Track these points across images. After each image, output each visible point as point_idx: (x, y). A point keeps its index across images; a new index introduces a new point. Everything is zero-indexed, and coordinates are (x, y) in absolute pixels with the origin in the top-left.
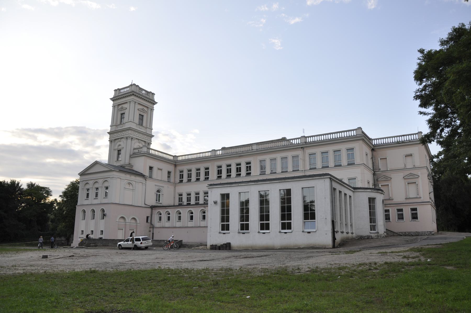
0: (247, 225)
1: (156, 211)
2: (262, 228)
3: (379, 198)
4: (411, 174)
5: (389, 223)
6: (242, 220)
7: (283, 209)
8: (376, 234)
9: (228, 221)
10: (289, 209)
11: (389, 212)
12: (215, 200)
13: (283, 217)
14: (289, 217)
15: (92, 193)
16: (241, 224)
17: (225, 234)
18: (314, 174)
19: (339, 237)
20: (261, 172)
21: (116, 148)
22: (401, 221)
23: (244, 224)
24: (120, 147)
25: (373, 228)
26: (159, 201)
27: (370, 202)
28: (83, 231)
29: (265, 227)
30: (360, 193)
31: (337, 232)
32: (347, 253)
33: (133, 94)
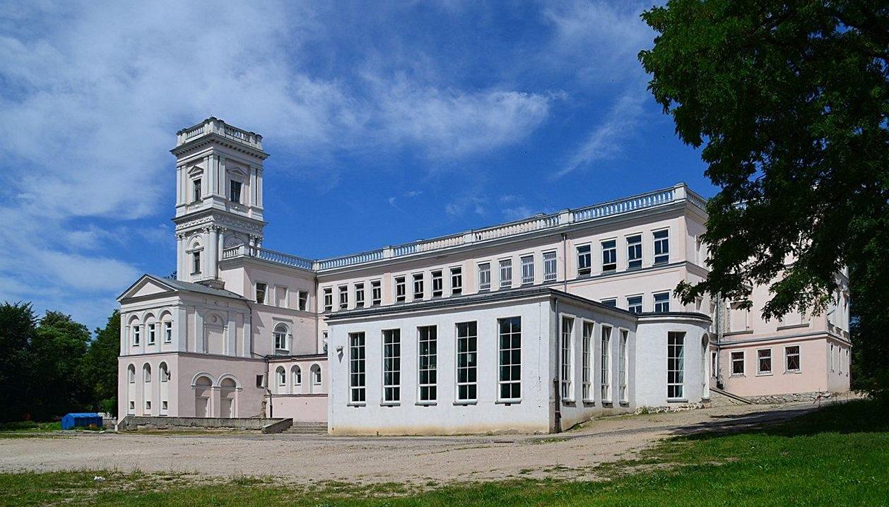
1: (273, 367)
2: (505, 394)
3: (693, 335)
5: (741, 379)
6: (355, 384)
7: (505, 358)
8: (683, 404)
9: (473, 378)
12: (339, 345)
13: (504, 375)
14: (517, 374)
15: (145, 333)
16: (503, 385)
17: (465, 405)
20: (503, 284)
21: (191, 248)
24: (197, 247)
25: (673, 392)
26: (283, 347)
28: (133, 403)
29: (429, 394)
31: (568, 404)
33: (213, 141)
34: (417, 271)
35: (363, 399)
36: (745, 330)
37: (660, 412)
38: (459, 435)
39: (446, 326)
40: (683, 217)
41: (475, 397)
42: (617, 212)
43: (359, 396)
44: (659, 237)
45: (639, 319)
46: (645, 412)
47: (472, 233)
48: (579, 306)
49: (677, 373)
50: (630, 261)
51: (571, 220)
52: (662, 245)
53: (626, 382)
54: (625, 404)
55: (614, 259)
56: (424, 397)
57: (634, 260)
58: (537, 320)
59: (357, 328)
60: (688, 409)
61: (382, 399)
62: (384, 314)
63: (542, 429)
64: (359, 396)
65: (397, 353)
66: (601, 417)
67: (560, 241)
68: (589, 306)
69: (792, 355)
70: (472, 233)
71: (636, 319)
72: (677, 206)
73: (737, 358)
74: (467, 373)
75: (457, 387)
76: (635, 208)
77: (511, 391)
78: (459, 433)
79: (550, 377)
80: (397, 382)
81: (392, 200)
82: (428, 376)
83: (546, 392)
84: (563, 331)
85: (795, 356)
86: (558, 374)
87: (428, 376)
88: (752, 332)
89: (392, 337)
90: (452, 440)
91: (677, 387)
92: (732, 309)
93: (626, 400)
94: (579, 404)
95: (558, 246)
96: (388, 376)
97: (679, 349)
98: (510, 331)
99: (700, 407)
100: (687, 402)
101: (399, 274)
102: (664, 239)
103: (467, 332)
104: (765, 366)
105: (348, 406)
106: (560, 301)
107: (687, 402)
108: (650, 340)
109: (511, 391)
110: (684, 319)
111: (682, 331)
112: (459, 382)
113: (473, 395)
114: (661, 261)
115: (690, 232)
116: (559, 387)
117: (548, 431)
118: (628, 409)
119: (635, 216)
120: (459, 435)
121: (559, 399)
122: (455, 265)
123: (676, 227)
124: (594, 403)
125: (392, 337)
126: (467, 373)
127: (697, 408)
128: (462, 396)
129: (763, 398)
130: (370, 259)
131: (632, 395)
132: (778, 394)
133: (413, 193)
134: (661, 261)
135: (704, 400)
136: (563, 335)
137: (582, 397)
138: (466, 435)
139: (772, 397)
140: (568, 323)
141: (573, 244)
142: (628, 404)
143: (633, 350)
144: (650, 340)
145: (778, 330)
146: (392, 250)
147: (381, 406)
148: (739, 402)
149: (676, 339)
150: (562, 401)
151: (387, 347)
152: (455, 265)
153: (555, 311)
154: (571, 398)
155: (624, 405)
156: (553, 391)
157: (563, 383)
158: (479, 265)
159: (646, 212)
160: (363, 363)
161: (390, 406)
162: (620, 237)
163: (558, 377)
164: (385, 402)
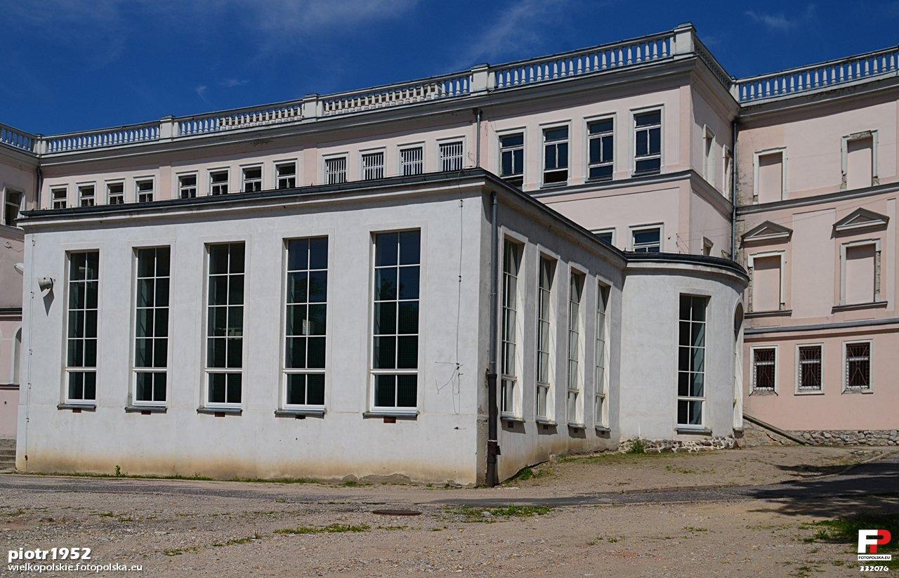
0: (236, 380)
2: (383, 398)
3: (721, 300)
4: (770, 227)
7: (384, 319)
8: (702, 438)
9: (236, 361)
10: (410, 319)
11: (819, 357)
13: (383, 356)
14: (410, 356)
17: (301, 416)
18: (574, 185)
19: (513, 448)
22: (809, 389)
23: (150, 374)
25: (688, 412)
27: (684, 314)
29: (307, 391)
30: (280, 259)
31: (512, 425)
32: (767, 501)
34: (218, 165)
35: (91, 394)
36: (777, 309)
37: (665, 450)
38: (287, 481)
39: (265, 242)
40: (687, 89)
41: (320, 401)
42: (571, 73)
43: (83, 387)
44: (645, 124)
45: (629, 265)
46: (638, 448)
47: (317, 101)
48: (537, 222)
49: (692, 374)
50: (592, 166)
51: (492, 85)
52: (649, 141)
53: (606, 389)
54: (603, 432)
55: (564, 163)
56: (216, 396)
57: (599, 165)
58: (453, 237)
59: (83, 240)
60: (712, 447)
61: (130, 396)
62: (138, 213)
63: (461, 476)
64: (83, 387)
65: (164, 298)
66: (569, 455)
67: (471, 123)
68: (552, 222)
69: (809, 362)
70: (317, 101)
71: (622, 263)
72: (677, 67)
73: (763, 360)
74: (307, 349)
75: (285, 377)
76: (604, 67)
77: (396, 392)
78: (287, 476)
79: (480, 363)
80: (162, 361)
81: (201, 89)
82: (225, 350)
83: (471, 397)
84: (505, 270)
85: (770, 366)
86: (495, 359)
87: (225, 350)
88: (788, 314)
89: (154, 262)
90: (271, 497)
91: (692, 402)
92: (755, 269)
93: (605, 423)
94: (530, 427)
95: (466, 133)
96: (143, 346)
97: (698, 329)
98: (398, 255)
99: (731, 445)
100: (710, 434)
101: (187, 169)
102: (652, 127)
103: (308, 258)
104: (811, 376)
105: (60, 408)
106: (502, 202)
107: (710, 434)
108: (649, 301)
109: (396, 392)
110: (709, 269)
111: (707, 294)
112: (288, 366)
113: (318, 397)
114: (648, 169)
115: (699, 118)
116: (494, 384)
117: (474, 481)
118: (608, 443)
119: (606, 80)
120: (287, 481)
121: (494, 419)
122: (284, 157)
123: (675, 104)
124: (554, 426)
125: (154, 262)
126: (307, 349)
127: (727, 447)
128: (295, 397)
129: (808, 436)
130: (137, 138)
131: (614, 417)
132: (832, 429)
133: (233, 82)
134: (648, 169)
135: (739, 434)
136: (505, 275)
137: (535, 413)
138: (301, 481)
139: (822, 435)
140: (514, 249)
141: (493, 129)
142: (554, 426)
143: (616, 326)
144: (649, 301)
145: (832, 313)
146: (176, 124)
147: (128, 410)
148: (784, 440)
149: (692, 307)
150: (501, 418)
151: (145, 286)
152: (284, 157)
153: (491, 223)
154: (517, 412)
155: (603, 433)
156: (485, 396)
157: (502, 381)
158: (327, 160)
159: (625, 75)
160: (93, 317)
161: (146, 412)
162: (576, 118)
163: (494, 366)
164: (136, 402)
